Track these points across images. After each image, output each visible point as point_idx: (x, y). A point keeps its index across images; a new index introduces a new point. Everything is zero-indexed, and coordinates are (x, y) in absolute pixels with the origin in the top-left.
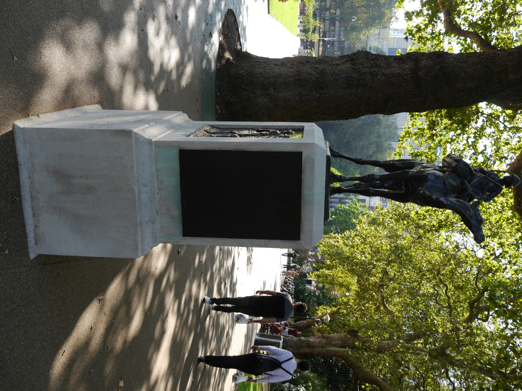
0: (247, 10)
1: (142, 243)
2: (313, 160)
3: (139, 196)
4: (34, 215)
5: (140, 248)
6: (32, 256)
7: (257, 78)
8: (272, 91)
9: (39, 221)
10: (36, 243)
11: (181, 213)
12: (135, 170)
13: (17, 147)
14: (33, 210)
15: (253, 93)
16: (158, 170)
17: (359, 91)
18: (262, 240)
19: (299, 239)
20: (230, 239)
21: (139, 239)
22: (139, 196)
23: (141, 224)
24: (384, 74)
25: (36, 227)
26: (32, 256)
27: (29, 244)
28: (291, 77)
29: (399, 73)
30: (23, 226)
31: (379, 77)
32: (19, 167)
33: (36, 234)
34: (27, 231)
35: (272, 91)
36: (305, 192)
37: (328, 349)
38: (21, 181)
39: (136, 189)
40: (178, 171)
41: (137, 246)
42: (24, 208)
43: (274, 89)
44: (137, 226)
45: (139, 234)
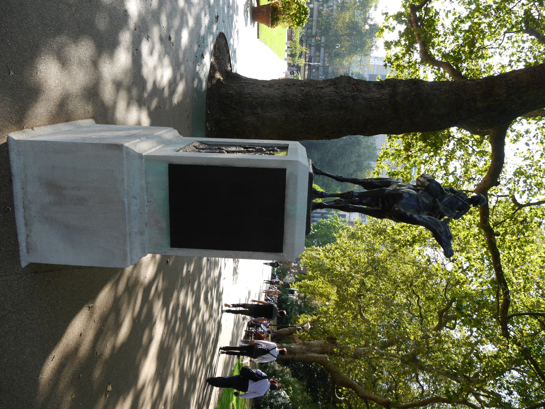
0: (238, 34)
1: (131, 253)
2: (296, 177)
3: (129, 208)
4: (26, 225)
5: (129, 258)
6: (24, 264)
7: (246, 98)
8: (260, 110)
9: (30, 231)
10: (28, 252)
11: (169, 225)
12: (126, 183)
13: (11, 159)
14: (25, 219)
15: (242, 112)
16: (147, 183)
17: (341, 113)
18: (247, 252)
19: (282, 251)
20: (215, 251)
21: (128, 249)
22: (129, 208)
23: (130, 235)
24: (364, 98)
25: (28, 236)
26: (24, 264)
27: (20, 252)
28: (278, 98)
29: (378, 98)
30: (16, 235)
31: (359, 101)
32: (13, 178)
33: (28, 243)
34: (19, 240)
35: (260, 110)
36: (288, 206)
37: (308, 355)
38: (15, 192)
39: (126, 201)
40: (167, 184)
41: (126, 256)
42: (16, 217)
43: (262, 109)
44: (126, 237)
45: (128, 244)
